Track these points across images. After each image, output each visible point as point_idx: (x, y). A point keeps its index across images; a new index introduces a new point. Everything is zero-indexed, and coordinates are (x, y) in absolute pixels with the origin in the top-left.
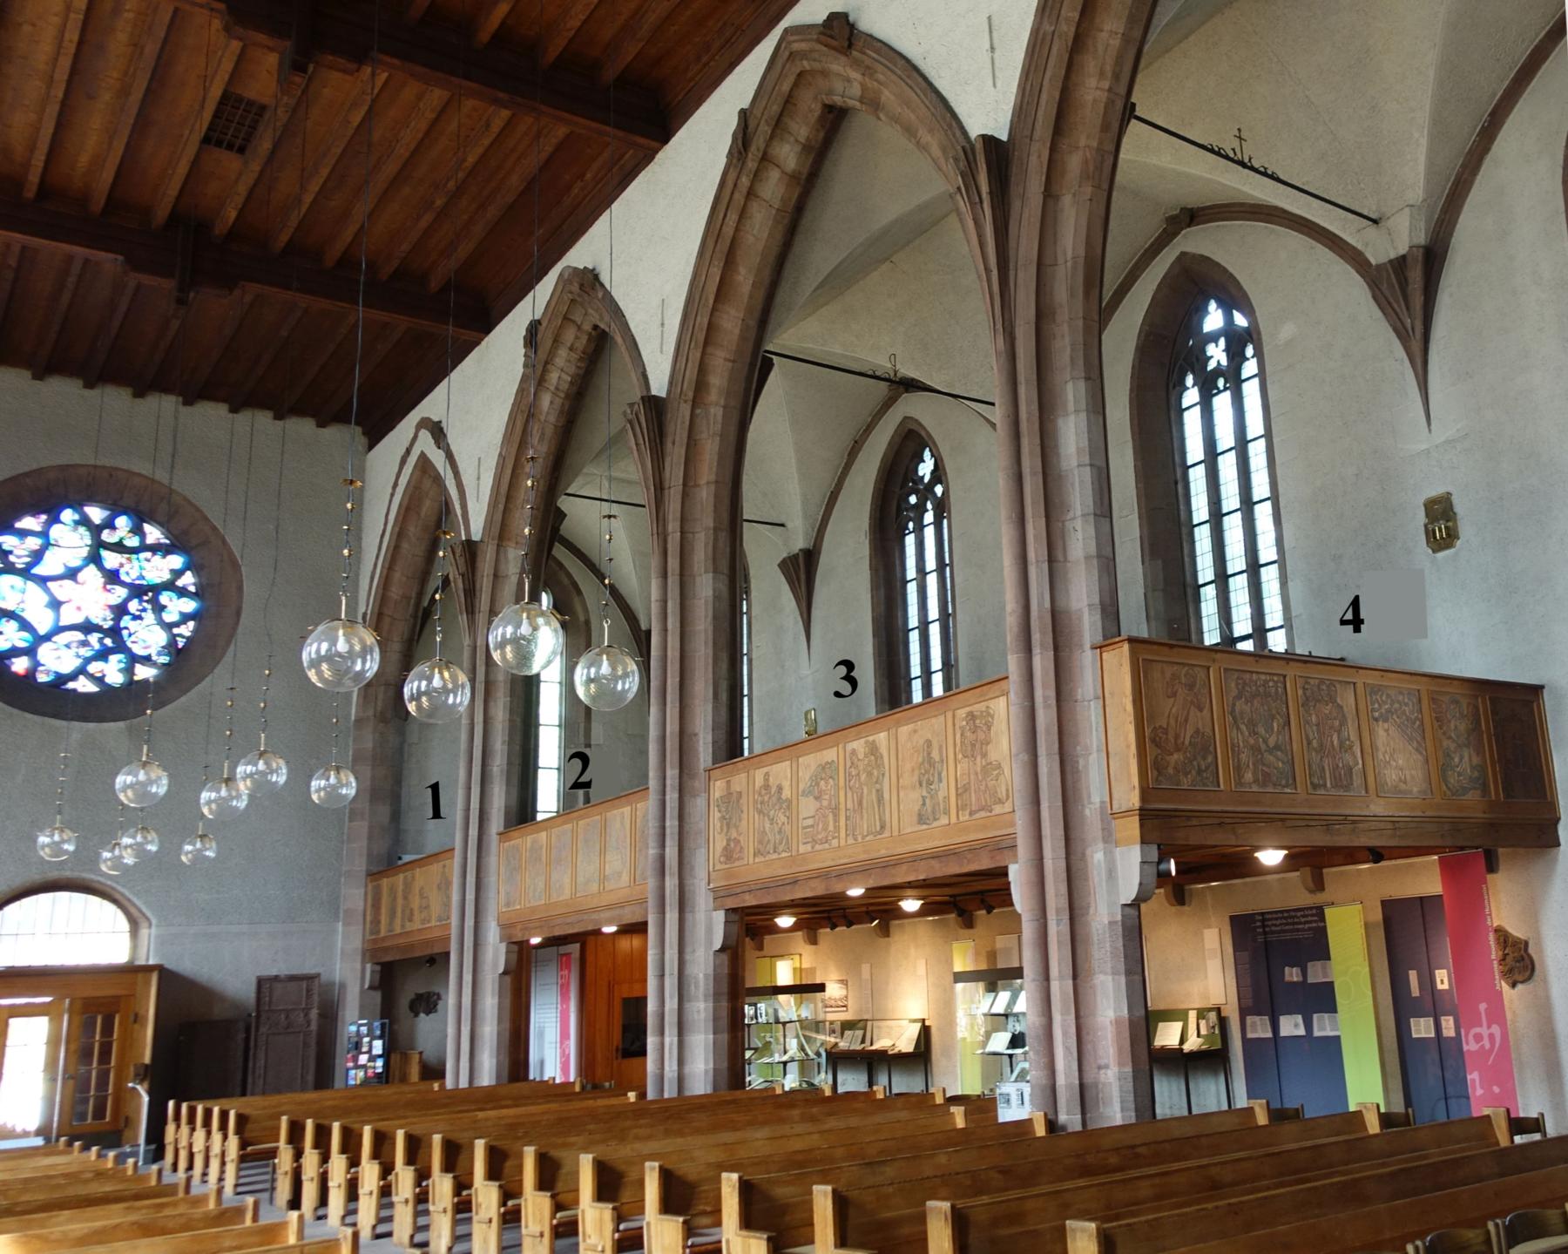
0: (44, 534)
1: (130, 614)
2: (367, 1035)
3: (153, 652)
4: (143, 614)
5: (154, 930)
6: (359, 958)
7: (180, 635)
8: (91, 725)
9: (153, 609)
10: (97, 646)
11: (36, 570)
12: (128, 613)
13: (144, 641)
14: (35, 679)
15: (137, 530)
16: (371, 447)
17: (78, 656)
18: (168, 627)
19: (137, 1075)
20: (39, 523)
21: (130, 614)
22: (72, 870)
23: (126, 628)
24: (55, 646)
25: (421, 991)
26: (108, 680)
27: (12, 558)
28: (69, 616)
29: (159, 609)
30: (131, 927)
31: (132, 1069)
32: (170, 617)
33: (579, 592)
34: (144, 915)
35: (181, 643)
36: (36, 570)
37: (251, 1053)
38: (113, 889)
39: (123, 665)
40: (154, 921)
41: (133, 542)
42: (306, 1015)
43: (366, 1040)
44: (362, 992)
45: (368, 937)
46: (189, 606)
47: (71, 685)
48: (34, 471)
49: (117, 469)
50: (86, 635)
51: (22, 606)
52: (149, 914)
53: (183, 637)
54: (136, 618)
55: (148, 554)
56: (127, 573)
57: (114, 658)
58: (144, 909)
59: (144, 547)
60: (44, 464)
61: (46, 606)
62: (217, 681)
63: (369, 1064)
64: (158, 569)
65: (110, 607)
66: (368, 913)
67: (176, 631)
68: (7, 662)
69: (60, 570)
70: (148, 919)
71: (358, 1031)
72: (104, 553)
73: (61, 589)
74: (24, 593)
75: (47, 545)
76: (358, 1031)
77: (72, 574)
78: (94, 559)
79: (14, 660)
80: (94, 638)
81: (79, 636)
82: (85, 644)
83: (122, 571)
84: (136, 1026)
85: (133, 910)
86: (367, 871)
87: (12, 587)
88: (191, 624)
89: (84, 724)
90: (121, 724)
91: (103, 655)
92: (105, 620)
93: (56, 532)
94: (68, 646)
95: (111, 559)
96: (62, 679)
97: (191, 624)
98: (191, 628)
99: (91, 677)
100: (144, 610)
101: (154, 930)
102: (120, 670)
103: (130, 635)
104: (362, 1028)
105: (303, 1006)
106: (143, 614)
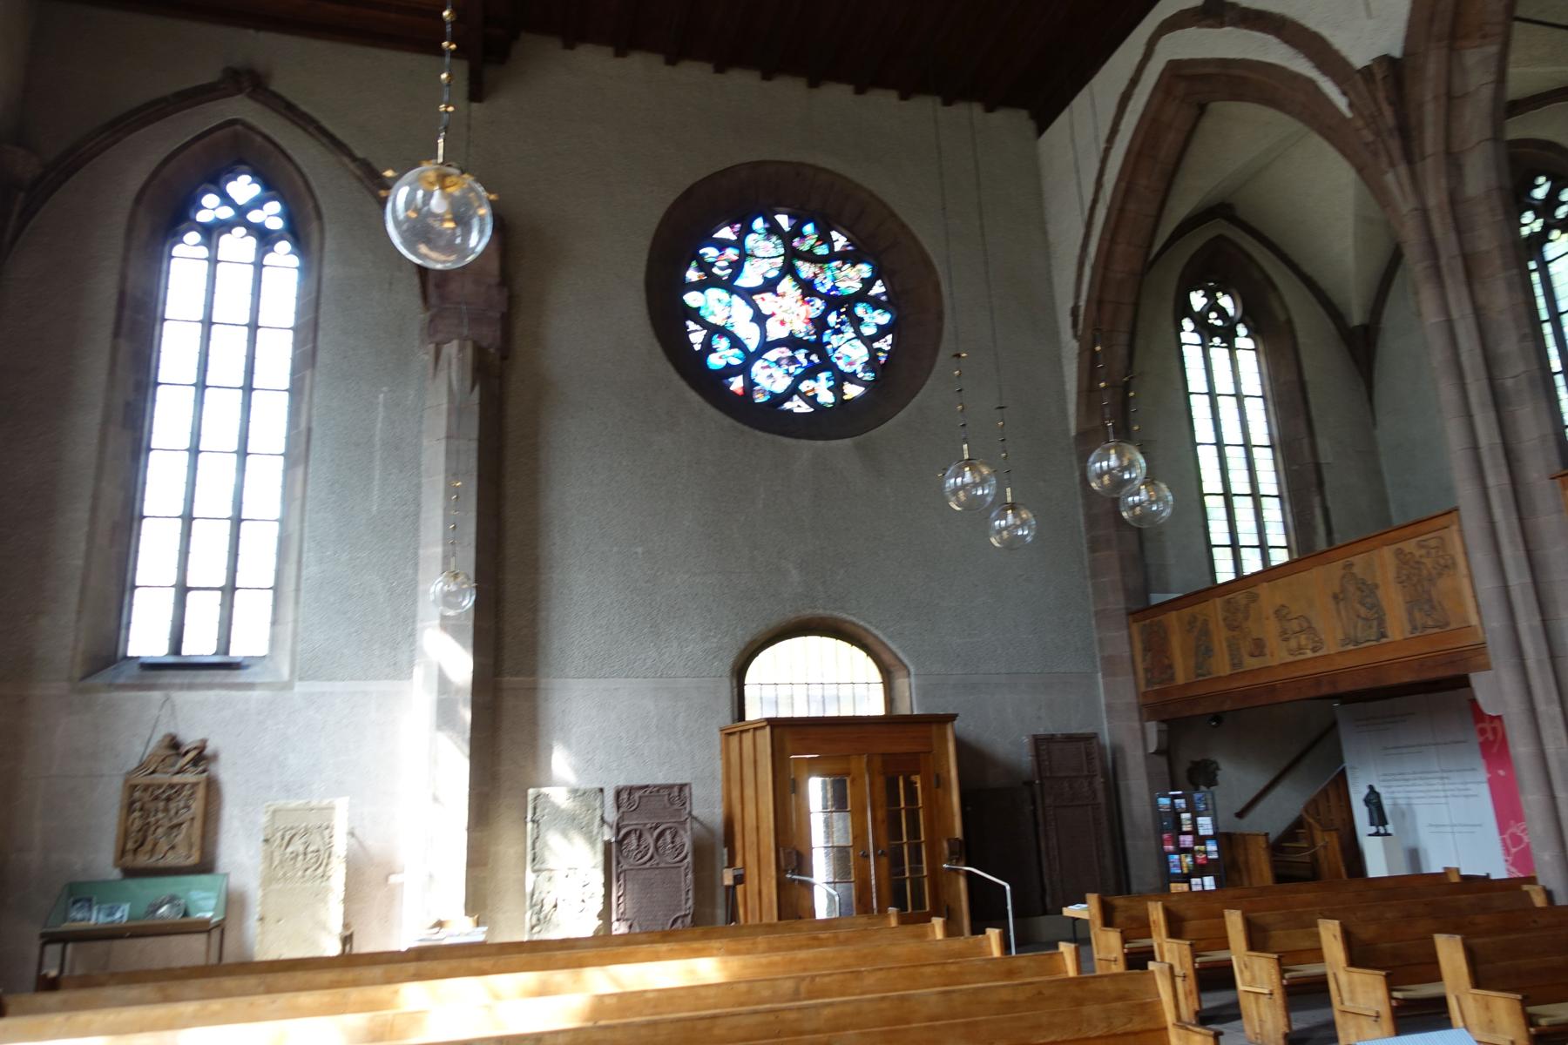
0: (739, 244)
1: (829, 328)
2: (1186, 811)
3: (858, 368)
4: (843, 328)
5: (913, 679)
6: (1136, 716)
7: (880, 350)
8: (820, 443)
9: (851, 322)
10: (805, 363)
11: (740, 282)
12: (828, 327)
13: (849, 357)
14: (752, 399)
15: (825, 238)
16: (1041, 130)
17: (789, 374)
18: (868, 341)
19: (952, 853)
20: (734, 233)
21: (829, 328)
22: (825, 609)
23: (829, 343)
24: (766, 364)
25: (1198, 759)
26: (820, 400)
27: (715, 270)
28: (775, 331)
29: (857, 322)
30: (883, 677)
31: (945, 845)
32: (868, 331)
33: (1274, 287)
34: (900, 661)
35: (882, 358)
36: (740, 282)
37: (1041, 828)
38: (866, 630)
39: (832, 383)
40: (912, 670)
41: (822, 250)
42: (1090, 783)
43: (1185, 816)
44: (1147, 756)
45: (1143, 689)
46: (884, 318)
47: (787, 406)
48: (729, 168)
49: (802, 164)
50: (793, 350)
51: (730, 321)
52: (906, 661)
53: (884, 351)
54: (838, 332)
55: (838, 263)
56: (823, 284)
57: (823, 376)
58: (901, 655)
59: (832, 256)
60: (737, 161)
61: (752, 320)
62: (933, 395)
63: (1197, 848)
64: (850, 278)
65: (811, 320)
66: (1139, 659)
67: (876, 345)
68: (725, 381)
69: (759, 282)
70: (905, 667)
71: (1173, 804)
72: (799, 263)
73: (766, 302)
74: (730, 306)
75: (744, 256)
76: (1173, 804)
77: (770, 286)
78: (788, 269)
79: (731, 380)
80: (801, 355)
81: (785, 352)
82: (793, 360)
83: (817, 281)
84: (940, 791)
85: (886, 657)
86: (1127, 609)
87: (719, 301)
88: (889, 338)
89: (812, 442)
90: (848, 441)
91: (811, 373)
92: (808, 334)
93: (750, 241)
94: (778, 363)
95: (806, 270)
96: (777, 399)
97: (889, 338)
98: (890, 342)
99: (803, 396)
100: (842, 323)
101: (913, 679)
102: (830, 389)
103: (834, 350)
104: (1177, 801)
105: (1086, 773)
106: (843, 328)
